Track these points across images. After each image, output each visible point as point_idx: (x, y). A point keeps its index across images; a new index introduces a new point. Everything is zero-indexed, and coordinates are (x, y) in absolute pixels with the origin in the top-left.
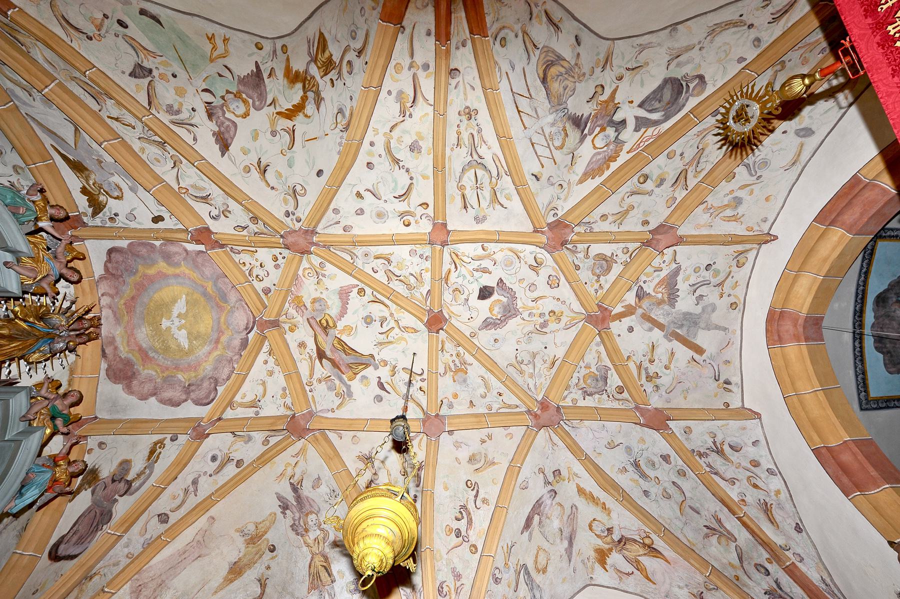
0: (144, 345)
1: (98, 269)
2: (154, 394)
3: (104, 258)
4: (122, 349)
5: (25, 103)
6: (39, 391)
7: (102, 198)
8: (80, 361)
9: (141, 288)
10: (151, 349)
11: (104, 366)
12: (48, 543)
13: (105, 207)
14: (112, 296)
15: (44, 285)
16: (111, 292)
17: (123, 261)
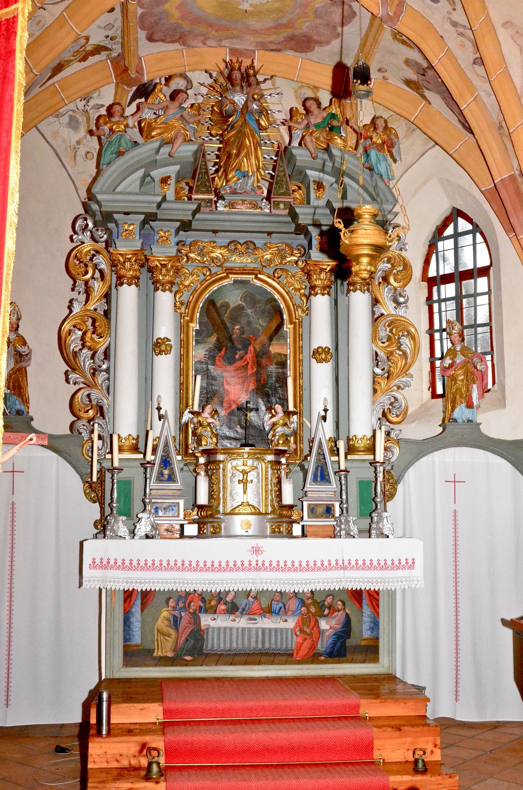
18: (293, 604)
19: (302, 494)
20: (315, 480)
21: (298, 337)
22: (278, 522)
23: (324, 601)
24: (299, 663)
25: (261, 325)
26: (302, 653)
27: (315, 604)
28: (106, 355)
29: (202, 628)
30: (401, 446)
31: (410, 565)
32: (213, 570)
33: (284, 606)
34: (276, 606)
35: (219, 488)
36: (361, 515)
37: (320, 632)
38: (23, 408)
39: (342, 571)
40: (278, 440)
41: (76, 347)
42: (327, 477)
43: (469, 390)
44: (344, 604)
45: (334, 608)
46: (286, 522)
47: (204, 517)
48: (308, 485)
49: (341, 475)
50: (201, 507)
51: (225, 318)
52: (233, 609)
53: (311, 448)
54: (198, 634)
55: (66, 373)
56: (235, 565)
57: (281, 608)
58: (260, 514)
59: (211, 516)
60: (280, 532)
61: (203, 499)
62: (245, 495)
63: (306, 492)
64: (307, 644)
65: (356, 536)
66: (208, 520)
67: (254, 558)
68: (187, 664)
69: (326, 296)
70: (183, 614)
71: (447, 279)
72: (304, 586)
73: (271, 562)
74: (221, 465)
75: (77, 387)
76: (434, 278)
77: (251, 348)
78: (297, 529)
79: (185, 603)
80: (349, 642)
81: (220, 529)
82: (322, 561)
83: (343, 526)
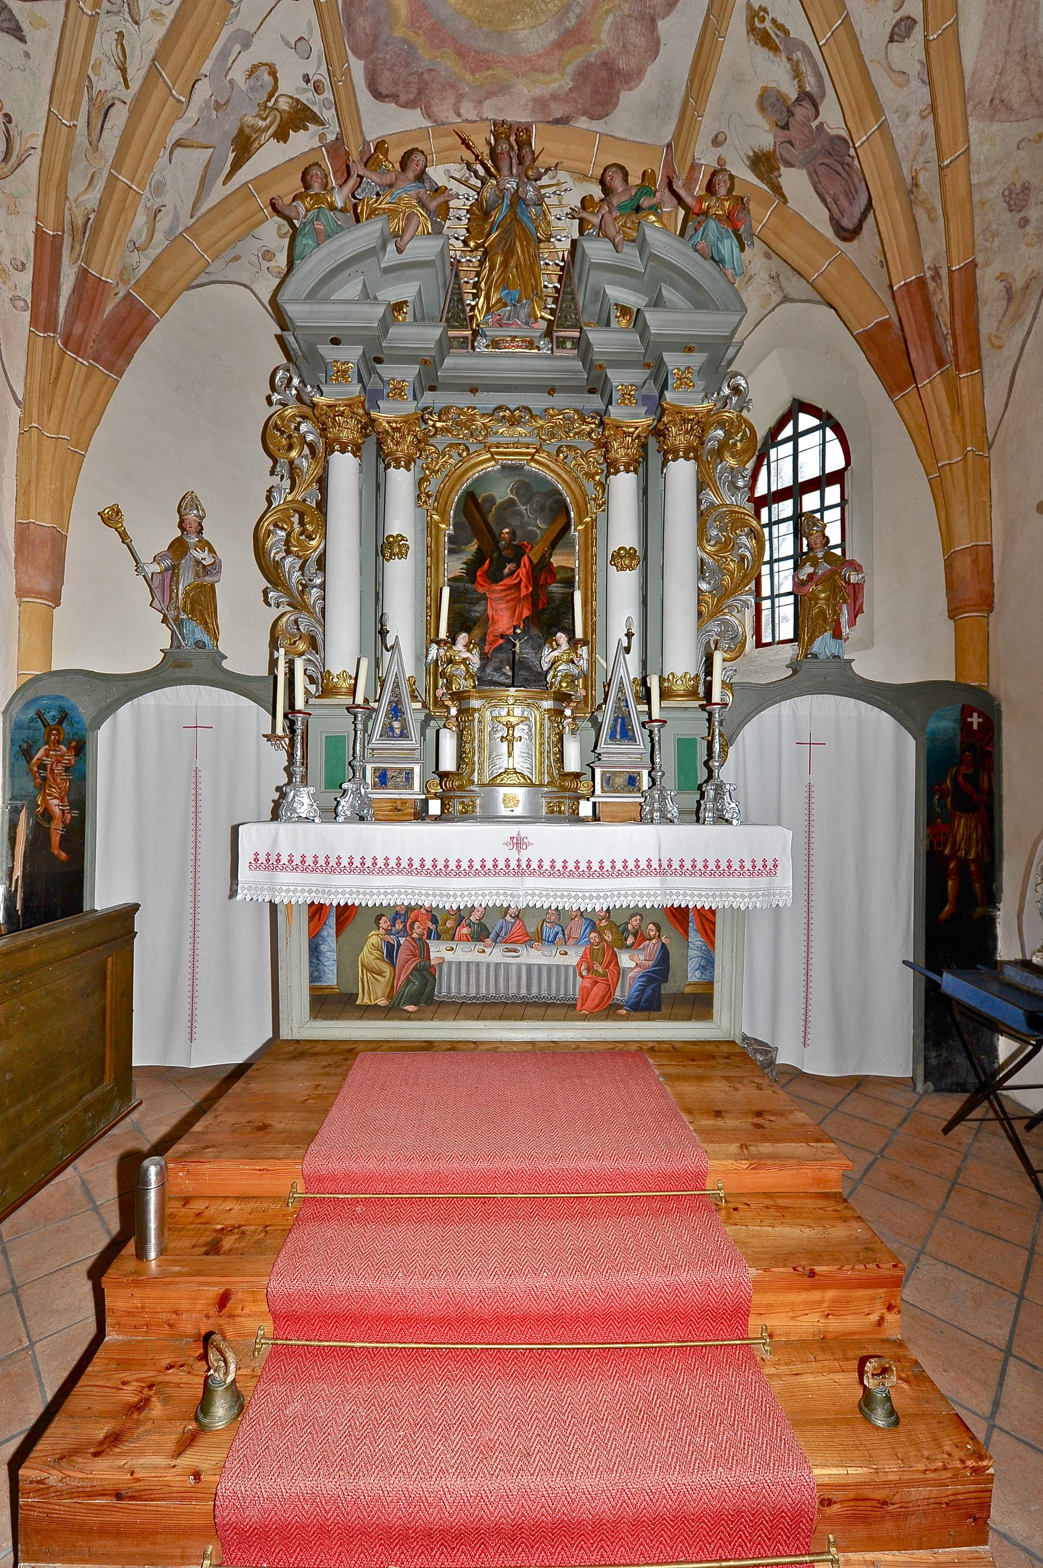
0: (553, 36)
1: (413, 120)
2: (653, 21)
3: (391, 107)
4: (556, 85)
5: (176, 218)
6: (593, 225)
7: (284, 105)
8: (566, 163)
9: (439, 35)
10: (560, 22)
11: (583, 123)
12: (828, 241)
13: (298, 101)
14: (460, 98)
15: (433, 205)
16: (453, 99)
17: (391, 70)
18: (577, 928)
19: (593, 755)
20: (612, 736)
21: (589, 540)
22: (558, 797)
23: (627, 923)
24: (585, 1018)
25: (539, 528)
26: (591, 1003)
27: (614, 928)
28: (321, 563)
29: (433, 963)
30: (735, 693)
31: (769, 869)
32: (447, 875)
33: (563, 931)
34: (549, 931)
35: (474, 748)
36: (681, 788)
37: (619, 972)
38: (206, 639)
39: (658, 879)
40: (560, 682)
41: (277, 553)
42: (630, 733)
43: (837, 613)
44: (659, 929)
45: (642, 934)
46: (569, 798)
47: (450, 790)
48: (602, 745)
49: (653, 727)
50: (443, 776)
51: (491, 518)
52: (480, 934)
53: (606, 694)
54: (426, 974)
55: (265, 592)
56: (483, 866)
57: (557, 934)
58: (532, 785)
59: (461, 788)
60: (560, 812)
61: (448, 763)
62: (511, 759)
63: (600, 754)
64: (598, 990)
65: (676, 820)
66: (456, 796)
67: (513, 856)
68: (409, 1017)
69: (632, 475)
70: (402, 940)
71: (780, 496)
72: (594, 900)
73: (541, 861)
74: (476, 715)
75: (281, 610)
76: (764, 497)
77: (525, 558)
78: (585, 809)
79: (405, 922)
80: (668, 988)
81: (474, 806)
82: (625, 862)
83: (656, 805)
